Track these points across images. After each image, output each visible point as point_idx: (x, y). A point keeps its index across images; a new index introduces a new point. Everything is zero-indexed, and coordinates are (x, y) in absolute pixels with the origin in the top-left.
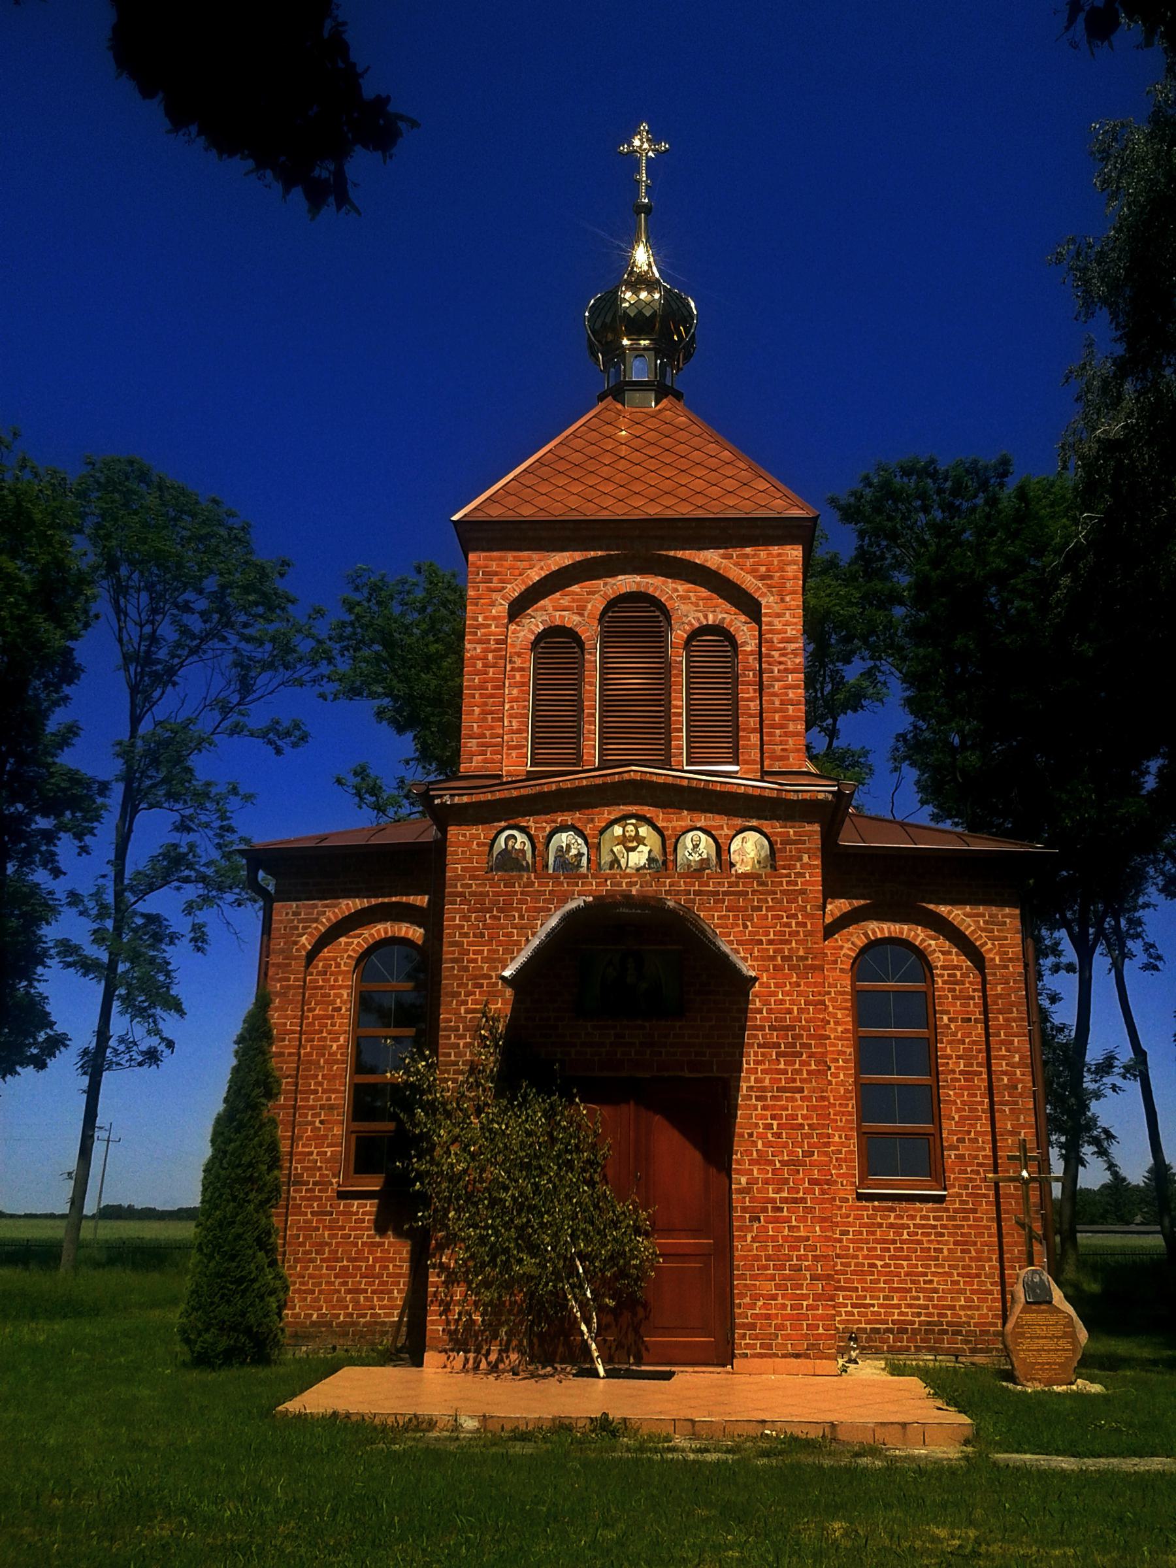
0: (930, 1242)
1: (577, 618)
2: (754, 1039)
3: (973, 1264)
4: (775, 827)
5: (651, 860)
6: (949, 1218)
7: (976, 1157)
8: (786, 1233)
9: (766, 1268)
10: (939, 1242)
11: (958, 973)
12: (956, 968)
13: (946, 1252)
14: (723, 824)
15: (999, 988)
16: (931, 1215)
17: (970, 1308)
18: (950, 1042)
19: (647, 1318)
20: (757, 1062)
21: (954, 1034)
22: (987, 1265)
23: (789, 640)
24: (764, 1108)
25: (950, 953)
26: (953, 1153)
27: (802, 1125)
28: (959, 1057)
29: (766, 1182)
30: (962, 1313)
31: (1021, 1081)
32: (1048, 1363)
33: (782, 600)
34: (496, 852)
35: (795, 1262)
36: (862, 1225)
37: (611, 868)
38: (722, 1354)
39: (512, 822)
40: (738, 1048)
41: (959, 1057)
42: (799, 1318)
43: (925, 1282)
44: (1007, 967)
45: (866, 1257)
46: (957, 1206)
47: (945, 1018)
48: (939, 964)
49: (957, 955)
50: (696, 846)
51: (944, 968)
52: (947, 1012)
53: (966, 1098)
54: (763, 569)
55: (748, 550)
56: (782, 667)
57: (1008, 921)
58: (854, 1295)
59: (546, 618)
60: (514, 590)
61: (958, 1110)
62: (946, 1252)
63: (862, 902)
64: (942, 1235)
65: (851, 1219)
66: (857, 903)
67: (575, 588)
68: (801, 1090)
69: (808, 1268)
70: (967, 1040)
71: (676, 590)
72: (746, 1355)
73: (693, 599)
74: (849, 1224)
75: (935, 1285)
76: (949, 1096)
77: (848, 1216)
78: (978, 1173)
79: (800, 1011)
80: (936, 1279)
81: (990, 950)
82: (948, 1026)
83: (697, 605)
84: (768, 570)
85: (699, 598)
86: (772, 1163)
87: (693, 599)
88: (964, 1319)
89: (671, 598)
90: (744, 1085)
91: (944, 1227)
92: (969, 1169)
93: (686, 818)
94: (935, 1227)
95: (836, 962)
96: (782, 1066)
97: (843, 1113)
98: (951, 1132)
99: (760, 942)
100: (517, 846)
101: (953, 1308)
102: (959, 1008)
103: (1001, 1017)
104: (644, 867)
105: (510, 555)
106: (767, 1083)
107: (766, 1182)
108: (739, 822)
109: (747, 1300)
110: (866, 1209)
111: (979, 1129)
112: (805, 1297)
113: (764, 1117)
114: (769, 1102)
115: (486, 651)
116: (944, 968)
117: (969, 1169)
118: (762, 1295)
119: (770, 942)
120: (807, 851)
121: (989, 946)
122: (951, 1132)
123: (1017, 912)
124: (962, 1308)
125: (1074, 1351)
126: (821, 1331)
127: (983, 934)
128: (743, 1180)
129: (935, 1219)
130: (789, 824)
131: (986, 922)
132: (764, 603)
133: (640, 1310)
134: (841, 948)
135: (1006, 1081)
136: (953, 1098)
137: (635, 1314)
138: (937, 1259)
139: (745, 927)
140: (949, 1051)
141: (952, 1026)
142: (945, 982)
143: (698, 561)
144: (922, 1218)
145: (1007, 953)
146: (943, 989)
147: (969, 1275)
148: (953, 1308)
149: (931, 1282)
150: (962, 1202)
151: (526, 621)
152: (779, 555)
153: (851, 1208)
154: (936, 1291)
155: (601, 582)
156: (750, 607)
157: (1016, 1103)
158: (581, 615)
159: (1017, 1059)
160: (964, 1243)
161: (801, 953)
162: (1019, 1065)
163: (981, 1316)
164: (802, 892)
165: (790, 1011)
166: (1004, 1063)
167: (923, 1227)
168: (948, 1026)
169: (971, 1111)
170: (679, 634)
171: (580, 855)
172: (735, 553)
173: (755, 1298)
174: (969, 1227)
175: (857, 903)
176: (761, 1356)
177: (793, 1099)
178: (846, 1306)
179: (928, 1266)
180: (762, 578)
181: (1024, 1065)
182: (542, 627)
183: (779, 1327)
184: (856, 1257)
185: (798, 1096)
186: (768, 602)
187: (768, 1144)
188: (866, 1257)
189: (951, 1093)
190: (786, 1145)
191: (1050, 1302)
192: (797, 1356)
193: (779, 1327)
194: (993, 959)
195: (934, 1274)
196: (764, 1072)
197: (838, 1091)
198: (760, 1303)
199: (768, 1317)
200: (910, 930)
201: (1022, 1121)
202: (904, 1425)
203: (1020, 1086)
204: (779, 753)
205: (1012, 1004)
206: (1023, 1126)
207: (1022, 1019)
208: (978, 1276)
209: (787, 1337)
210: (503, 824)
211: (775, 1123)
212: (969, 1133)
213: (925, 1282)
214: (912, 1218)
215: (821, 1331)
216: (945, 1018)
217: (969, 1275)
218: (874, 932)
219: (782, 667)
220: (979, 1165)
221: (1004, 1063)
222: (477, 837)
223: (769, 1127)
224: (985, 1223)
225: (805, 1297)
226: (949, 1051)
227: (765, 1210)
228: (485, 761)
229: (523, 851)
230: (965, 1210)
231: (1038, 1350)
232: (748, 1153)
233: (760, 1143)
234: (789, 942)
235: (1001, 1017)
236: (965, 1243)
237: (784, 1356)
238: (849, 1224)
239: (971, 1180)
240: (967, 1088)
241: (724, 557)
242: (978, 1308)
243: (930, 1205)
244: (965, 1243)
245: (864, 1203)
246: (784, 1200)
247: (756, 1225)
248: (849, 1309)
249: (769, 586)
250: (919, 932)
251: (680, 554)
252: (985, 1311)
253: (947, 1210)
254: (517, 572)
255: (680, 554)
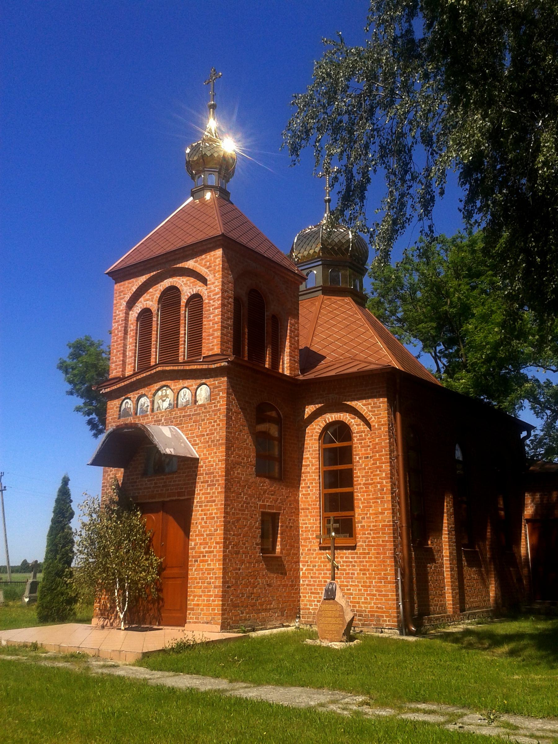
0: (349, 569)
1: (151, 303)
2: (200, 479)
3: (368, 581)
4: (210, 381)
5: (170, 404)
6: (358, 558)
7: (370, 526)
8: (206, 567)
9: (198, 583)
10: (353, 570)
11: (363, 434)
12: (364, 432)
13: (356, 574)
14: (193, 383)
15: (377, 439)
16: (350, 556)
17: (366, 603)
18: (359, 469)
19: (163, 606)
20: (200, 490)
21: (361, 465)
22: (374, 581)
23: (216, 294)
24: (202, 511)
25: (360, 425)
26: (360, 525)
27: (214, 517)
28: (363, 477)
29: (201, 544)
30: (363, 605)
31: (385, 486)
32: (331, 630)
33: (215, 276)
34: (122, 409)
35: (209, 580)
36: (321, 562)
37: (157, 410)
38: (181, 622)
39: (126, 396)
40: (194, 484)
41: (363, 477)
42: (209, 605)
43: (347, 590)
44: (380, 429)
45: (323, 578)
46: (361, 551)
47: (357, 457)
48: (355, 431)
49: (363, 425)
50: (185, 395)
51: (357, 433)
52: (358, 455)
53: (365, 497)
54: (208, 263)
55: (203, 256)
56: (213, 307)
57: (381, 405)
58: (318, 596)
59: (141, 306)
60: (128, 297)
61: (363, 503)
62: (356, 574)
63: (320, 405)
64: (354, 566)
65: (317, 559)
66: (318, 406)
67: (151, 290)
68: (214, 501)
69: (213, 583)
70: (367, 468)
71: (183, 281)
72: (190, 622)
73: (189, 284)
74: (316, 562)
75: (351, 591)
76: (358, 496)
77: (316, 558)
78: (370, 534)
79: (217, 465)
80: (352, 588)
81: (373, 421)
82: (358, 462)
83: (189, 286)
84: (210, 264)
85: (191, 283)
86: (203, 535)
87: (189, 284)
88: (364, 609)
89: (181, 285)
90: (195, 501)
91: (356, 562)
92: (367, 533)
93: (181, 383)
94: (351, 562)
95: (312, 436)
96: (209, 491)
97: (314, 508)
98: (359, 514)
99: (204, 435)
100: (129, 406)
101: (358, 603)
102: (363, 452)
103: (377, 454)
104: (167, 408)
105: (127, 282)
106: (203, 499)
107: (201, 544)
108: (199, 381)
109: (192, 597)
110: (323, 554)
111: (371, 512)
112: (211, 596)
113: (201, 515)
114: (204, 508)
115: (119, 325)
116: (357, 433)
117: (367, 533)
118: (197, 595)
119: (207, 435)
120: (221, 390)
121: (373, 419)
122: (359, 514)
123: (386, 400)
124: (363, 603)
125: (343, 624)
126: (216, 612)
127: (370, 414)
128: (193, 544)
129: (352, 558)
130: (216, 379)
131: (372, 407)
132: (208, 279)
133: (161, 602)
134: (315, 429)
135: (379, 487)
136: (360, 497)
137: (159, 603)
138: (352, 578)
139: (199, 429)
140: (359, 474)
141: (360, 461)
142: (358, 440)
143: (186, 267)
144: (346, 558)
145: (380, 422)
146: (357, 443)
147: (365, 586)
148: (358, 603)
149: (350, 589)
150: (364, 549)
151: (135, 309)
152: (214, 255)
153: (317, 554)
154: (351, 594)
155: (159, 285)
156: (204, 280)
157: (383, 498)
158: (152, 301)
159: (384, 475)
160: (364, 570)
161: (218, 438)
162: (385, 478)
163: (371, 607)
164: (219, 410)
165: (212, 466)
166: (378, 477)
167: (346, 562)
168: (358, 462)
169: (368, 503)
170: (184, 300)
171: (148, 406)
172: (198, 259)
173: (194, 596)
174: (367, 562)
175: (318, 406)
176: (195, 623)
177: (211, 506)
178: (314, 601)
179: (348, 582)
180: (208, 268)
181: (387, 478)
182: (140, 310)
183: (202, 610)
184: (319, 577)
185: (213, 504)
186: (210, 278)
187: (202, 527)
188: (323, 578)
189: (359, 495)
190: (208, 527)
191: (334, 599)
192: (207, 623)
193: (202, 610)
194: (375, 426)
195: (351, 586)
196: (203, 494)
197: (312, 498)
198: (196, 599)
199: (198, 605)
200: (344, 416)
201: (386, 507)
202: (120, 651)
203: (385, 489)
204: (211, 347)
205: (382, 447)
206: (385, 509)
207: (387, 455)
208: (370, 586)
209: (204, 614)
210: (123, 398)
211: (205, 517)
212: (367, 514)
213: (347, 590)
214: (342, 558)
215: (216, 612)
216: (357, 457)
217: (365, 586)
218: (329, 419)
219: (213, 307)
220: (371, 530)
221: (378, 477)
222: (115, 404)
223: (203, 519)
224: (373, 559)
225: (211, 596)
226: (359, 474)
227: (199, 557)
228: (117, 372)
229: (130, 408)
230: (364, 553)
231: (328, 624)
232: (195, 531)
233: (199, 526)
234: (213, 433)
235: (377, 454)
236: (364, 570)
237: (203, 623)
238: (316, 562)
239: (367, 538)
240: (366, 492)
241: (196, 262)
242: (370, 603)
243: (350, 551)
244: (364, 570)
245: (322, 551)
246: (207, 552)
247: (196, 563)
248: (316, 603)
249: (210, 271)
250: (347, 416)
251: (178, 266)
252: (373, 605)
253: (356, 554)
254: (129, 289)
255: (178, 266)
